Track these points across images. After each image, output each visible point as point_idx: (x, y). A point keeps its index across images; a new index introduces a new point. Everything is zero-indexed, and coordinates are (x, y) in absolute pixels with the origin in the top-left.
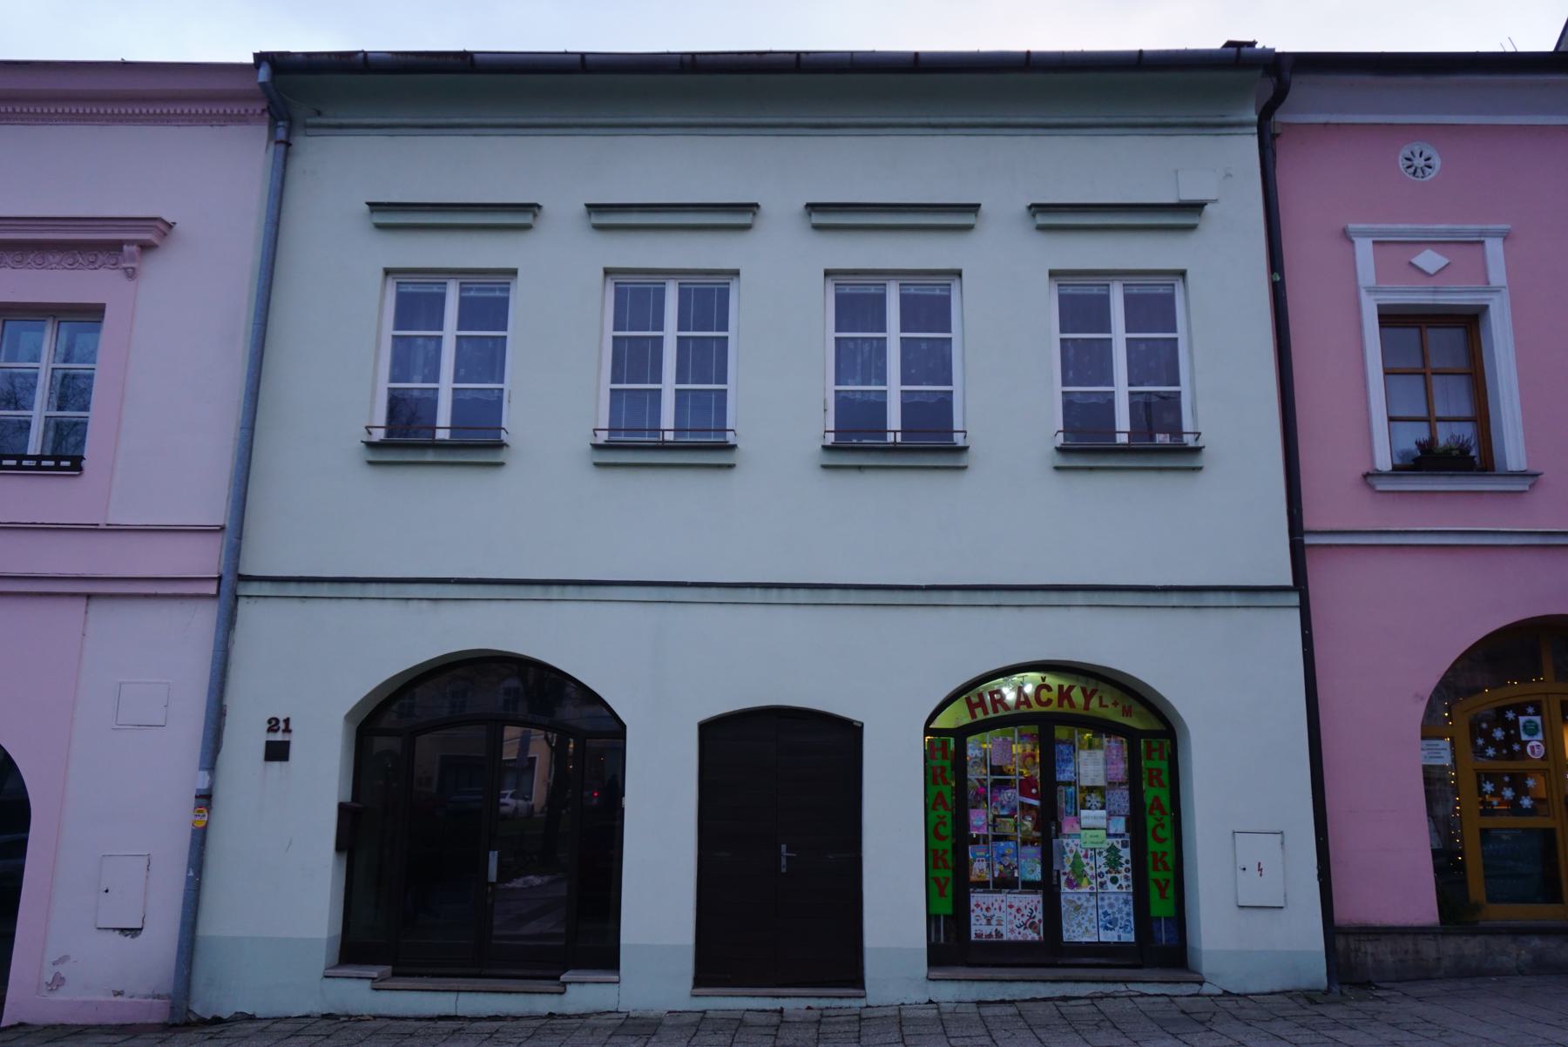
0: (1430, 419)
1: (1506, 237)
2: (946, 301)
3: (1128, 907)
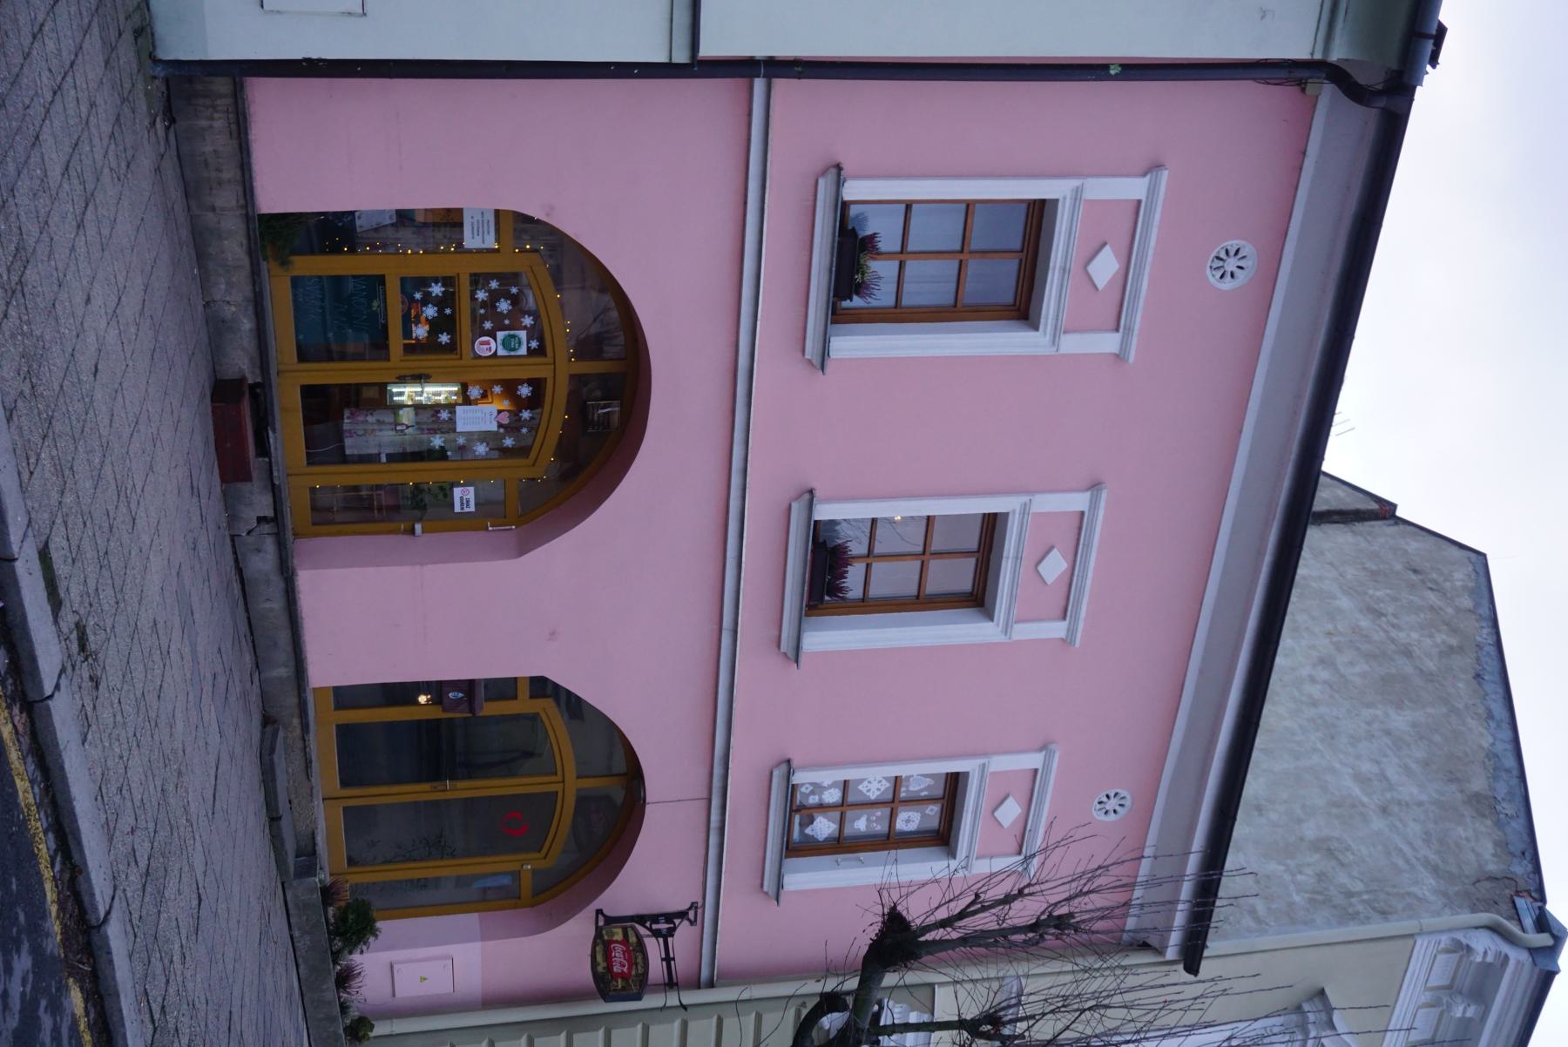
0: (903, 254)
1: (1119, 358)
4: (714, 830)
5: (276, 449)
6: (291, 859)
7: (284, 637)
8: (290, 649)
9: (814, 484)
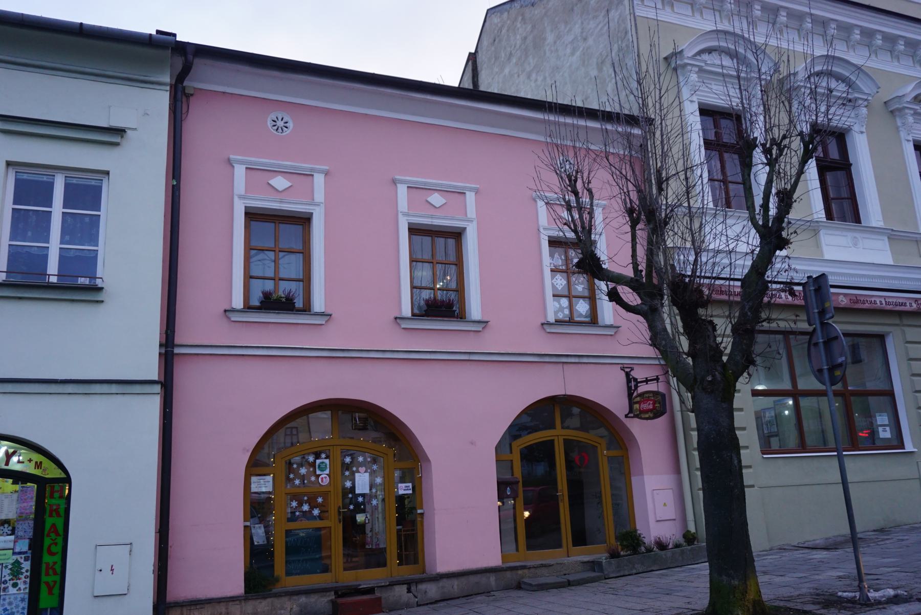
1: (327, 174)
2: (99, 189)
3: (24, 603)
4: (579, 360)
5: (370, 584)
6: (593, 574)
7: (473, 579)
8: (479, 576)
9: (392, 317)
